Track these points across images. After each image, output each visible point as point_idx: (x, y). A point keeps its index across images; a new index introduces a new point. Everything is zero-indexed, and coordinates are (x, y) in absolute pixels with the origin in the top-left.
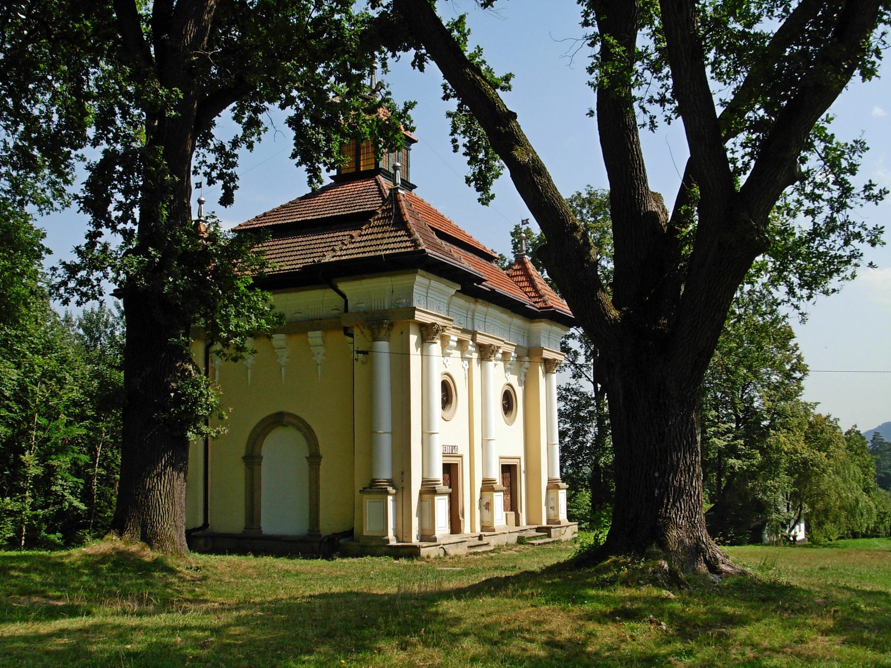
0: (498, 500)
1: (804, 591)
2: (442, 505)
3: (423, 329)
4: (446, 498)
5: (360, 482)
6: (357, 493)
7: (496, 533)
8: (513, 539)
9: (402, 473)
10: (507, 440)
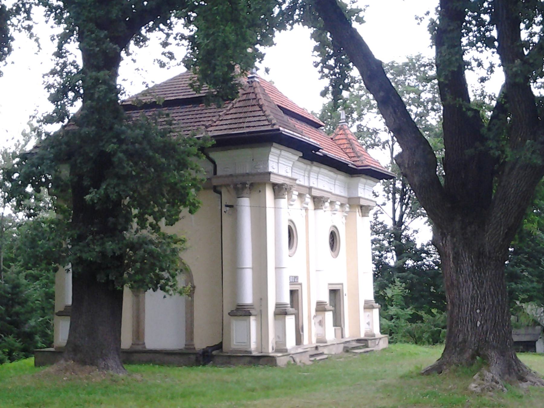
0: (329, 316)
2: (290, 321)
4: (293, 317)
5: (227, 308)
7: (328, 344)
8: (340, 349)
9: (261, 299)
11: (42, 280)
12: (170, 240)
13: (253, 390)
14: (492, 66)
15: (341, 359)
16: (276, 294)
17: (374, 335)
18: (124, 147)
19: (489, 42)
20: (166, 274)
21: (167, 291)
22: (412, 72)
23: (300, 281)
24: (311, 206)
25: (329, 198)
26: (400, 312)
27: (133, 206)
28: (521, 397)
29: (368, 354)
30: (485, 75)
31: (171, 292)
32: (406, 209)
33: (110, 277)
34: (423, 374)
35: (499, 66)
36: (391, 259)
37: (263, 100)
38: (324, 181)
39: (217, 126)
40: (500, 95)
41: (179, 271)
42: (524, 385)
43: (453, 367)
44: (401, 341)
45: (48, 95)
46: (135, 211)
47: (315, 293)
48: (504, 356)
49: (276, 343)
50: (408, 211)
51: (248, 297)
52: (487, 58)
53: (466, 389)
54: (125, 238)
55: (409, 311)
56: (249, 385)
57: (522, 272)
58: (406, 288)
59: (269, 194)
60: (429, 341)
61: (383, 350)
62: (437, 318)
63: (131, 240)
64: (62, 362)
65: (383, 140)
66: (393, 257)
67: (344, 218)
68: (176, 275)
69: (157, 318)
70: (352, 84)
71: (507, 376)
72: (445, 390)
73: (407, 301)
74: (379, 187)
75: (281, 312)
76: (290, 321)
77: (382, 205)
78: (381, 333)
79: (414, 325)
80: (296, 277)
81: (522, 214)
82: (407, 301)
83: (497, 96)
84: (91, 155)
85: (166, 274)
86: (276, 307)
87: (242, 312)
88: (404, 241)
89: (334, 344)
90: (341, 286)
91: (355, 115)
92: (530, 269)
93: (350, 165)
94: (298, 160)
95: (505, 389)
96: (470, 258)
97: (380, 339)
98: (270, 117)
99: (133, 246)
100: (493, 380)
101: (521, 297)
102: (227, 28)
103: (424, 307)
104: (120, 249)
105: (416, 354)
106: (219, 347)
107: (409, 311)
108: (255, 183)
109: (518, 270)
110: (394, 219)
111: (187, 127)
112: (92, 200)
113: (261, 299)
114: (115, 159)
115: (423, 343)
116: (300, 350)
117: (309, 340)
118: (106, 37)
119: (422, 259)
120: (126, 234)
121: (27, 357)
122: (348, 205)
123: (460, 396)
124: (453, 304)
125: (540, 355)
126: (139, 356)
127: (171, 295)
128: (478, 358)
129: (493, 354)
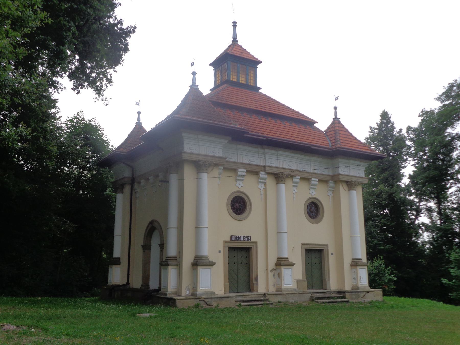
97: (368, 292)
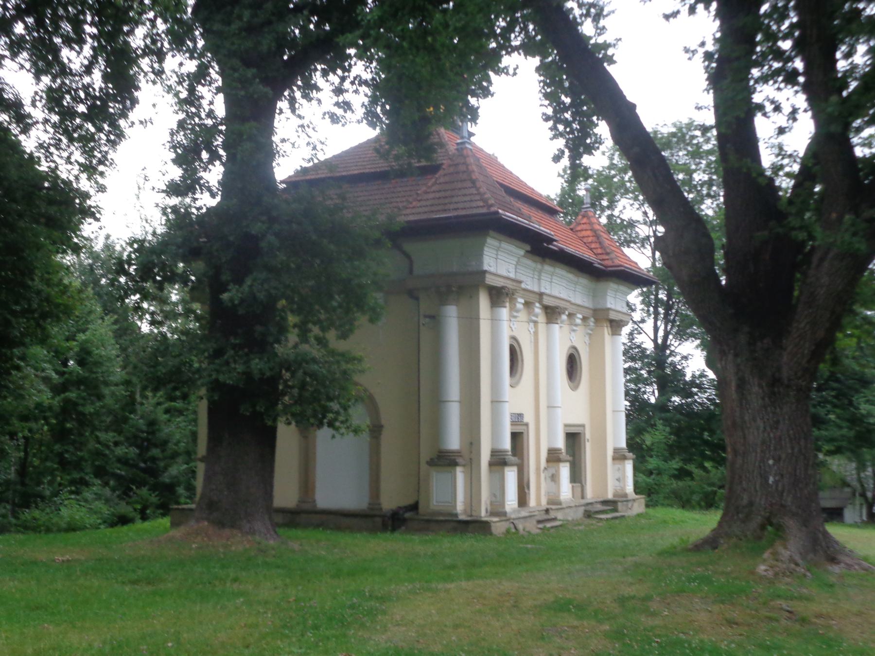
0: (565, 471)
1: (94, 207)
2: (511, 476)
3: (549, 311)
4: (515, 469)
5: (426, 454)
6: (424, 466)
7: (564, 506)
9: (471, 443)
10: (570, 407)
11: (187, 416)
12: (340, 358)
13: (453, 567)
14: (794, 111)
15: (580, 528)
16: (493, 437)
17: (626, 495)
18: (277, 227)
19: (791, 78)
20: (335, 406)
21: (337, 429)
22: (682, 146)
23: (526, 420)
24: (542, 319)
25: (566, 309)
26: (662, 465)
27: (292, 311)
28: (831, 586)
29: (617, 521)
30: (784, 125)
31: (343, 430)
32: (671, 329)
33: (258, 408)
34: (690, 550)
35: (805, 111)
36: (651, 394)
37: (477, 174)
38: (560, 286)
39: (414, 207)
40: (806, 154)
41: (353, 401)
42: (836, 569)
43: (734, 540)
44: (663, 505)
45: (173, 156)
46: (292, 319)
47: (546, 437)
48: (806, 526)
49: (492, 503)
50: (675, 330)
51: (454, 441)
52: (788, 99)
53: (752, 572)
54: (276, 355)
55: (675, 464)
56: (448, 561)
57: (826, 415)
58: (671, 434)
59: (484, 302)
60: (699, 504)
61: (639, 515)
62: (712, 475)
63: (285, 356)
64: (192, 522)
65: (642, 235)
66: (653, 392)
67: (587, 338)
68: (349, 407)
69: (329, 466)
70: (597, 145)
71: (811, 556)
72: (723, 573)
73: (672, 450)
74: (635, 297)
75: (499, 461)
76: (511, 476)
77: (640, 322)
78: (636, 493)
79: (680, 484)
80: (520, 415)
81: (836, 325)
82: (672, 450)
83: (801, 155)
84: (231, 238)
85: (335, 406)
86: (492, 456)
87: (445, 460)
88: (668, 371)
89: (571, 507)
90: (582, 428)
91: (605, 203)
92: (838, 411)
93: (597, 265)
94: (524, 256)
95: (808, 574)
96: (760, 386)
97: (634, 500)
98: (486, 196)
99: (287, 365)
100: (792, 560)
101: (826, 447)
102: (418, 60)
103: (695, 460)
104: (271, 369)
105: (682, 521)
106: (414, 507)
107: (675, 464)
108: (466, 285)
109: (821, 412)
110: (655, 341)
111: (373, 209)
112: (231, 300)
113: (471, 443)
114: (263, 244)
115: (693, 508)
116: (524, 513)
117: (537, 500)
118: (254, 77)
119: (692, 395)
120: (279, 349)
121: (163, 515)
122: (592, 319)
123: (744, 583)
124: (735, 452)
125: (851, 526)
126: (305, 516)
127: (342, 434)
128: (769, 528)
129: (791, 524)
